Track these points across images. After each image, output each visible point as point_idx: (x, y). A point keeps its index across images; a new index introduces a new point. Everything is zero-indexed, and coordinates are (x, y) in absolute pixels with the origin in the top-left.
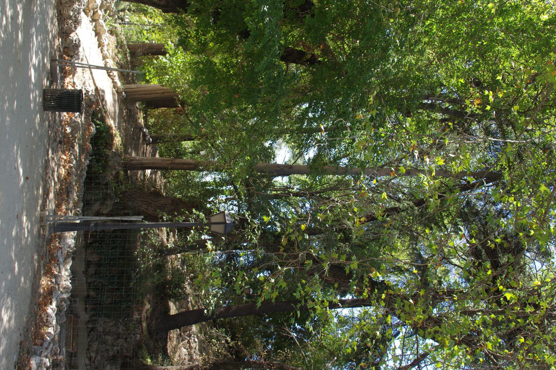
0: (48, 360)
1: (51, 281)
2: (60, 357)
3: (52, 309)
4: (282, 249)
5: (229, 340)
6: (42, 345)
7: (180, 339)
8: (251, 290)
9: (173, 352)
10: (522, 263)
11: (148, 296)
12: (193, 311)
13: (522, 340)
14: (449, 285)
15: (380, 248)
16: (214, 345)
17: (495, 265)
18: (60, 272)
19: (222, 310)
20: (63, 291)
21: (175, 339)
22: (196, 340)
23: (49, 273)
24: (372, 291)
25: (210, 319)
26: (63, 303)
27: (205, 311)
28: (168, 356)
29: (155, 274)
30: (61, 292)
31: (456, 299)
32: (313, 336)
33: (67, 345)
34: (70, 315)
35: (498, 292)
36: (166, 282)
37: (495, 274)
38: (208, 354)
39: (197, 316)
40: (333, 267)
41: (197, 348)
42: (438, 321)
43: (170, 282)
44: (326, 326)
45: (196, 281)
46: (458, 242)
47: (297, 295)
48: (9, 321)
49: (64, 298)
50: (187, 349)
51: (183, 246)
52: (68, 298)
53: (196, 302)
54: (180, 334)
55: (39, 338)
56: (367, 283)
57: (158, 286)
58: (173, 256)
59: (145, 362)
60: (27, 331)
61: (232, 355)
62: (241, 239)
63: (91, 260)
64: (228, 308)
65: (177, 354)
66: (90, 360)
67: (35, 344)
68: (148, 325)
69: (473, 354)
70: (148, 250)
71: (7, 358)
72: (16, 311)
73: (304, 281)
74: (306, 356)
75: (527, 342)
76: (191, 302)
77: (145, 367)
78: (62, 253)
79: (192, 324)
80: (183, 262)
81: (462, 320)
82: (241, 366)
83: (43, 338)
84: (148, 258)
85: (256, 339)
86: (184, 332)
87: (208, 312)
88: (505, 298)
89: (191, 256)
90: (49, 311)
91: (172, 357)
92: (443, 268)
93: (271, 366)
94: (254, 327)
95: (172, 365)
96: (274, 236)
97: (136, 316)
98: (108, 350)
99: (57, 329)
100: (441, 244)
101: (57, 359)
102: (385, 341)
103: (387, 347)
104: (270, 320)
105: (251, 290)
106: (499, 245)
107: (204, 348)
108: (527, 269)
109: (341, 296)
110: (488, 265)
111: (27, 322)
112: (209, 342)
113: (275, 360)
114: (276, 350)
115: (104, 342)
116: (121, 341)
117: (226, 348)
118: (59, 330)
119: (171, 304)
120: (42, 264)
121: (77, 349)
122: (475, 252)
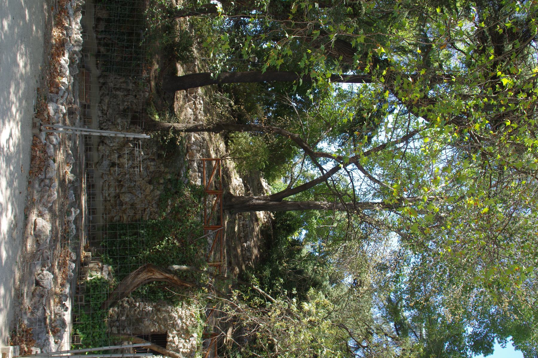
0: (64, 107)
1: (62, 33)
2: (75, 106)
3: (64, 60)
4: (291, 17)
5: (233, 103)
6: (57, 93)
7: (187, 100)
8: (256, 58)
9: (179, 111)
10: (526, 52)
11: (157, 56)
12: (200, 74)
13: (508, 123)
14: (449, 70)
15: (387, 27)
16: (218, 108)
17: (499, 51)
18: (70, 25)
19: (227, 75)
20: (75, 44)
21: (181, 99)
22: (202, 102)
23: (60, 24)
24: (374, 66)
25: (215, 83)
26: (75, 56)
27: (212, 75)
28: (175, 114)
29: (164, 35)
30: (73, 45)
31: (454, 80)
32: (312, 108)
33: (80, 97)
34: (82, 69)
35: (495, 77)
36: (174, 44)
37: (497, 59)
38: (211, 115)
39: (202, 80)
40: (339, 40)
41: (202, 109)
42: (432, 101)
43: (179, 44)
44: (326, 99)
45: (204, 45)
46: (467, 26)
47: (301, 64)
48: (25, 66)
49: (76, 51)
50: (193, 110)
51: (192, 9)
52: (80, 51)
53: (202, 66)
54: (187, 95)
55: (55, 86)
56: (370, 58)
57: (166, 48)
58: (182, 19)
59: (153, 118)
60: (43, 79)
61: (234, 117)
62: (251, 5)
63: (101, 16)
64: (233, 74)
65: (183, 114)
66: (103, 112)
67: (51, 92)
68: (156, 84)
69: (461, 132)
70: (156, 10)
71: (26, 101)
72: (30, 59)
73: (309, 51)
74: (304, 125)
75: (513, 125)
76: (198, 66)
77: (153, 123)
78: (71, 5)
79: (198, 87)
80: (192, 26)
81: (455, 102)
82: (242, 129)
83: (58, 87)
84: (157, 18)
85: (258, 105)
86: (190, 93)
87: (214, 75)
88: (501, 85)
89: (200, 20)
90: (62, 62)
91: (178, 116)
92: (447, 52)
93: (271, 131)
94: (257, 95)
95: (178, 122)
96: (283, 5)
97: (145, 75)
98: (119, 105)
99: (70, 79)
100: (449, 26)
101: (72, 107)
102: (380, 114)
103: (382, 121)
104: (272, 89)
105: (256, 58)
106: (508, 30)
107: (209, 110)
108: (529, 59)
109: (343, 72)
110: (492, 51)
111: (42, 70)
112: (214, 104)
113: (275, 126)
114: (275, 117)
115: (115, 97)
116: (131, 98)
117: (229, 112)
118: (72, 81)
119: (179, 66)
120: (52, 15)
121: (90, 101)
122: (480, 35)
